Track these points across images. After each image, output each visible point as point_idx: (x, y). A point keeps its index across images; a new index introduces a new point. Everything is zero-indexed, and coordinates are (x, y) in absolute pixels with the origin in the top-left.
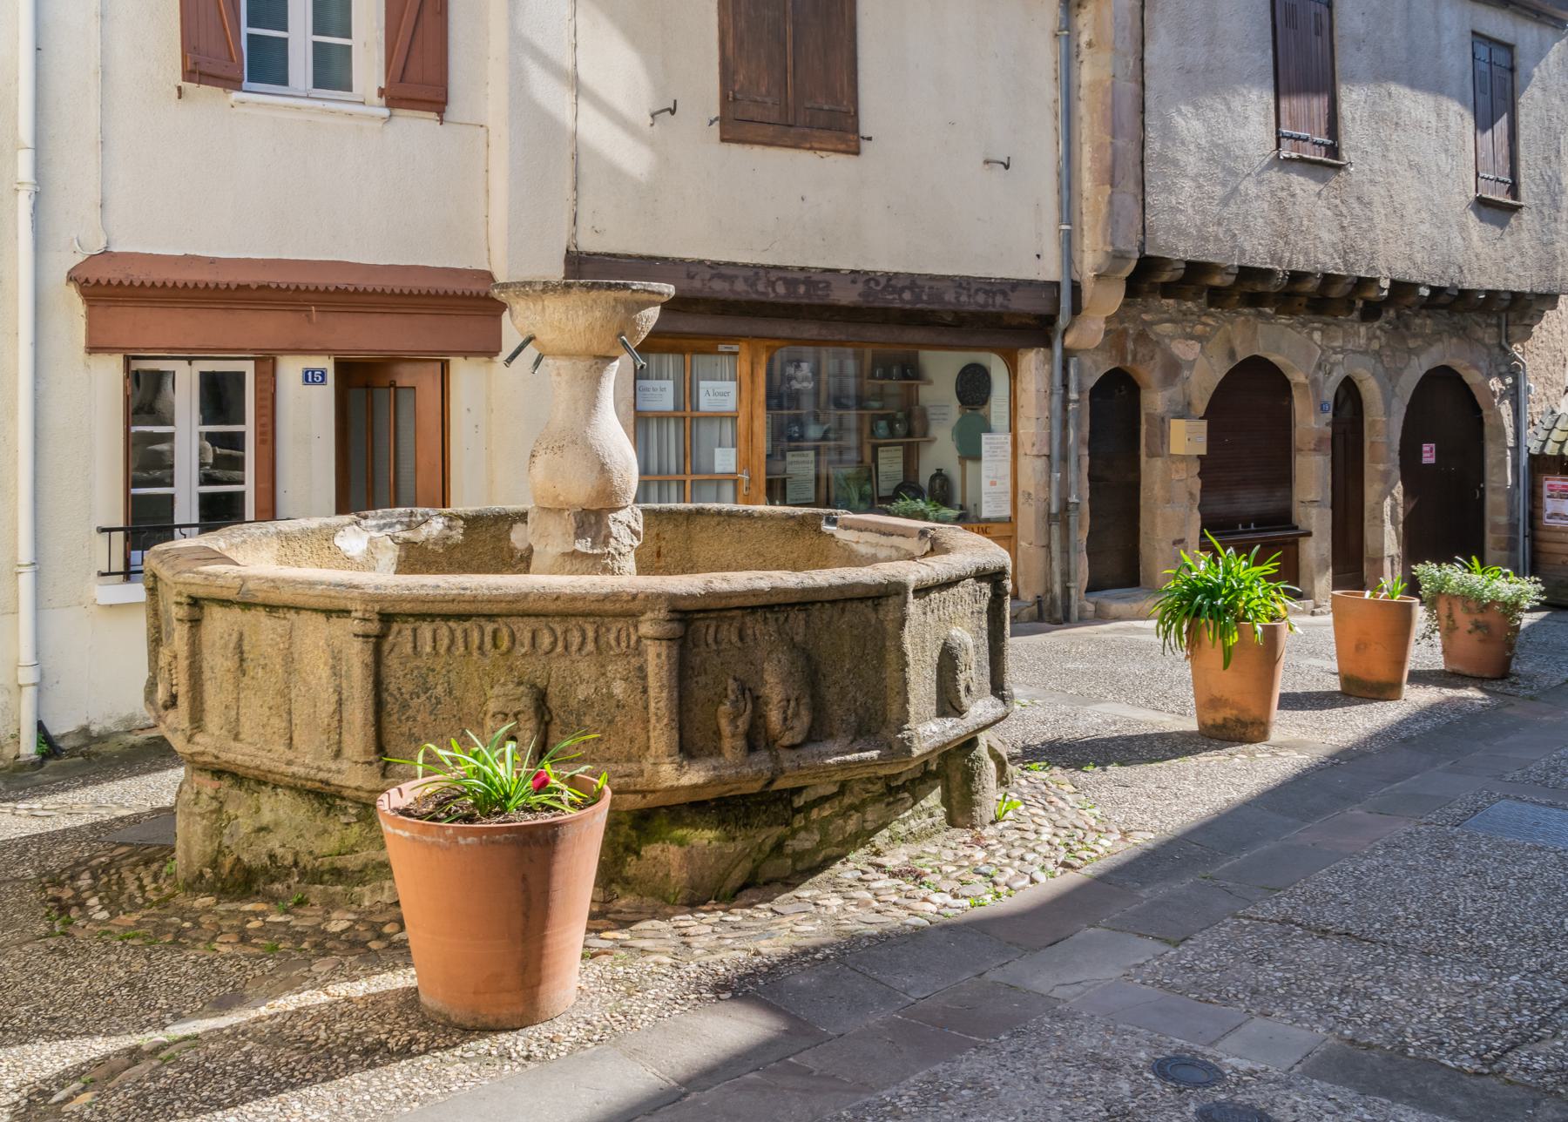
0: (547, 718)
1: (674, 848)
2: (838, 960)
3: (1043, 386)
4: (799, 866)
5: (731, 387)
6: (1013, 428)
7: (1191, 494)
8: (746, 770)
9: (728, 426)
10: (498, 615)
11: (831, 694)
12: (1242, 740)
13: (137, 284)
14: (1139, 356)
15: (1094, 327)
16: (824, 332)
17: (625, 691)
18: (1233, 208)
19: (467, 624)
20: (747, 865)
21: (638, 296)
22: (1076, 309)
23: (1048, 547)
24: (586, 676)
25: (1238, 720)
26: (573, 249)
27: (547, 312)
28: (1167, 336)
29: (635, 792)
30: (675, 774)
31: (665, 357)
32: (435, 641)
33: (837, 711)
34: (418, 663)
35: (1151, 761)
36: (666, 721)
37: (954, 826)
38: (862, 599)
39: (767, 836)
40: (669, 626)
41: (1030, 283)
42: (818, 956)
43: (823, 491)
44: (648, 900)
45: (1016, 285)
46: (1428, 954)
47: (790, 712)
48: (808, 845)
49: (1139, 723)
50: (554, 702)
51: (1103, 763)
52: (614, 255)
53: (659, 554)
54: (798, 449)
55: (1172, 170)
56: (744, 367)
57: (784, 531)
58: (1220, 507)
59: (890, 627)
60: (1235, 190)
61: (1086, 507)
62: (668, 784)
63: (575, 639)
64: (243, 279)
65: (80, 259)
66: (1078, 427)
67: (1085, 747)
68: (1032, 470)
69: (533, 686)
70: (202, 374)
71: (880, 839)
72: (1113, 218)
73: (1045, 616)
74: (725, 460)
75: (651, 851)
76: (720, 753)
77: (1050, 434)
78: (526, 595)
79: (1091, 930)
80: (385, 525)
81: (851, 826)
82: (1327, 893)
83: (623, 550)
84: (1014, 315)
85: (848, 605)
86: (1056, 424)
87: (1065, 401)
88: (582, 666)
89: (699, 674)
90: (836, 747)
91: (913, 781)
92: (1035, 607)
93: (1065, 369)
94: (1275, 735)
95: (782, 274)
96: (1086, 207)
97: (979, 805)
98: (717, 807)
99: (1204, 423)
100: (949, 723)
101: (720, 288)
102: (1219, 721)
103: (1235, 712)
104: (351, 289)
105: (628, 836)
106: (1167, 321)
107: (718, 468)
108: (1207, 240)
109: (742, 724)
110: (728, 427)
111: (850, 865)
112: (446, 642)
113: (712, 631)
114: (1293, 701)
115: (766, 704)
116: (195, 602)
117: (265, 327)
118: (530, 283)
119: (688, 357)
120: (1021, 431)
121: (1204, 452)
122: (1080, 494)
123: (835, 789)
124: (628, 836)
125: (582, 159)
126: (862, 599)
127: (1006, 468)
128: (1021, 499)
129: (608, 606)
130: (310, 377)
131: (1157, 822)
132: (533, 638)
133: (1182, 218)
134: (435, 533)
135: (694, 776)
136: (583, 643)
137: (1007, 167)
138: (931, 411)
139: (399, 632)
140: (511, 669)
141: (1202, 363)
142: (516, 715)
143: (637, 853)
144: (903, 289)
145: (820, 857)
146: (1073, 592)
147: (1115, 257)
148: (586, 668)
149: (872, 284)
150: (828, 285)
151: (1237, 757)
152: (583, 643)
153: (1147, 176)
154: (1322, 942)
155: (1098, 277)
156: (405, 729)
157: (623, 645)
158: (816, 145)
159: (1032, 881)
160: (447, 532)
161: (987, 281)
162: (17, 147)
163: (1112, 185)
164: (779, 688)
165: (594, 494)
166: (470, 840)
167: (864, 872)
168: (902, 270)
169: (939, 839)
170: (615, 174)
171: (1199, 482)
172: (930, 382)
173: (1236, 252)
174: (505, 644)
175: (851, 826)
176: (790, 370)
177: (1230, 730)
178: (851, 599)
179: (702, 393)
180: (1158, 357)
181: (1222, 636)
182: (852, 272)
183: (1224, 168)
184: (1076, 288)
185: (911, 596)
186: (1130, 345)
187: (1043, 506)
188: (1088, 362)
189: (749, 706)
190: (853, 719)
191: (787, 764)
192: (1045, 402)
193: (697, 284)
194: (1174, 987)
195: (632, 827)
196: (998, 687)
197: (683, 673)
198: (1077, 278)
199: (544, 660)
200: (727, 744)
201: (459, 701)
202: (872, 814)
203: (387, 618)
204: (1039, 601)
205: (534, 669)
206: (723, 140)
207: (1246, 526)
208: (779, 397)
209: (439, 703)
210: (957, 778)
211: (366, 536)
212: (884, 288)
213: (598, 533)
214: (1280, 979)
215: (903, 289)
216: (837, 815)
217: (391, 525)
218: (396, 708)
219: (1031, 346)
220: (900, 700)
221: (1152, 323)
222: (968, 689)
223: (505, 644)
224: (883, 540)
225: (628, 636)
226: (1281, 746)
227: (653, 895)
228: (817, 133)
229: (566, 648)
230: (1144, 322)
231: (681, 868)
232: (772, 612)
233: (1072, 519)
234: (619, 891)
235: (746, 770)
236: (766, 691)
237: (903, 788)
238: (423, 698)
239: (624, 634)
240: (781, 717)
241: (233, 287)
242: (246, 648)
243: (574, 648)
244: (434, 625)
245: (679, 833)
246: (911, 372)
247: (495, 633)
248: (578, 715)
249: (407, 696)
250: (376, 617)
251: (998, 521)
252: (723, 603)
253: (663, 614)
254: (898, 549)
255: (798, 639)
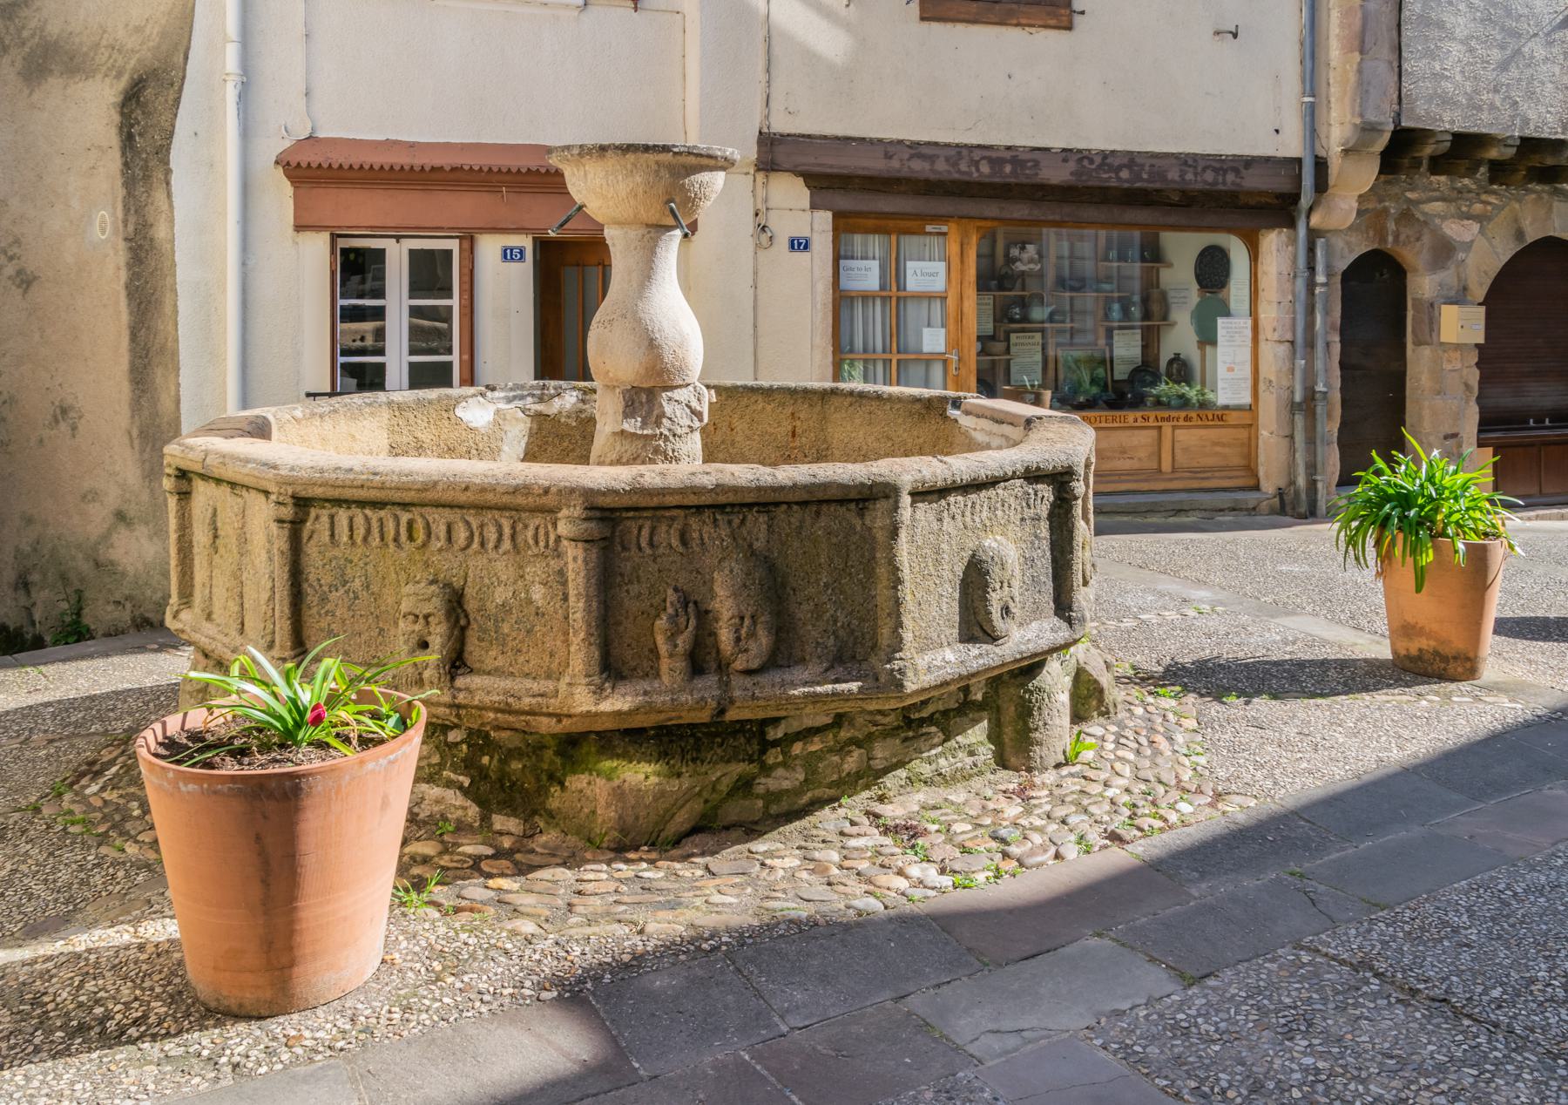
0: (463, 622)
1: (600, 782)
2: (726, 954)
3: (1286, 268)
4: (774, 809)
5: (941, 267)
6: (1254, 313)
7: (1467, 385)
8: (684, 697)
9: (937, 305)
10: (413, 505)
11: (803, 612)
12: (1443, 677)
13: (335, 166)
14: (1402, 237)
15: (1344, 206)
16: (1036, 212)
17: (544, 598)
18: (1514, 72)
19: (382, 513)
20: (697, 806)
21: (682, 159)
22: (1321, 185)
23: (1291, 437)
24: (504, 578)
25: (1436, 653)
26: (765, 130)
27: (590, 176)
28: (1439, 216)
29: (550, 715)
30: (591, 698)
31: (871, 237)
32: (351, 529)
33: (811, 632)
34: (336, 552)
35: (1313, 695)
36: (582, 635)
37: (1005, 767)
38: (842, 502)
39: (727, 773)
40: (585, 525)
41: (1268, 159)
42: (705, 946)
43: (1051, 373)
44: (572, 840)
45: (1250, 162)
46: (1556, 1057)
47: (743, 632)
48: (786, 785)
49: (1324, 642)
50: (471, 605)
51: (1247, 695)
52: (809, 136)
53: (794, 435)
54: (1023, 330)
55: (1436, 33)
56: (954, 248)
57: (911, 414)
58: (1505, 399)
59: (880, 536)
60: (1518, 52)
61: (1336, 396)
62: (584, 708)
63: (491, 535)
64: (457, 160)
65: (287, 144)
66: (1327, 312)
67: (1183, 682)
68: (1273, 356)
69: (448, 585)
70: (412, 252)
71: (891, 781)
72: (1363, 86)
73: (1288, 509)
74: (933, 340)
75: (577, 782)
76: (658, 675)
77: (1294, 319)
78: (436, 483)
79: (1094, 942)
80: (515, 398)
81: (852, 762)
82: (1446, 924)
83: (679, 431)
84: (1250, 193)
85: (824, 508)
86: (1300, 309)
87: (1311, 285)
88: (500, 565)
89: (631, 582)
90: (806, 676)
91: (945, 713)
92: (1277, 500)
93: (1311, 250)
94: (1490, 670)
95: (987, 153)
96: (1333, 77)
97: (1040, 744)
98: (657, 736)
99: (1483, 309)
100: (975, 650)
101: (919, 167)
102: (1414, 652)
103: (1432, 643)
104: (543, 171)
105: (552, 762)
106: (1437, 200)
107: (926, 349)
108: (1480, 109)
109: (683, 642)
110: (937, 306)
111: (841, 812)
112: (392, 533)
113: (645, 532)
114: (1513, 628)
115: (717, 620)
116: (183, 475)
117: (463, 206)
118: (568, 148)
119: (894, 238)
120: (1262, 316)
121: (1482, 341)
122: (1330, 382)
123: (828, 720)
124: (552, 762)
125: (773, 43)
126: (842, 502)
127: (1246, 354)
128: (1262, 387)
129: (520, 500)
130: (508, 254)
131: (1269, 784)
132: (449, 531)
133: (1449, 86)
134: (568, 406)
135: (619, 702)
136: (500, 540)
137: (1235, 36)
138: (1171, 294)
139: (317, 518)
140: (427, 565)
141: (1481, 243)
142: (426, 617)
143: (561, 784)
144: (1120, 168)
145: (805, 799)
146: (1320, 485)
147: (1363, 129)
148: (503, 568)
149: (1086, 162)
150: (1036, 164)
151: (1426, 699)
152: (500, 540)
153: (1404, 40)
154: (1399, 1010)
155: (1346, 152)
156: (323, 624)
157: (542, 544)
158: (1023, 21)
159: (1057, 856)
160: (581, 405)
161: (1217, 158)
162: (226, 40)
163: (1361, 52)
164: (729, 603)
165: (642, 371)
166: (191, 787)
167: (853, 823)
168: (1118, 148)
169: (977, 783)
170: (811, 58)
171: (1477, 372)
172: (1170, 265)
173: (1518, 121)
174: (420, 536)
175: (852, 762)
176: (1015, 252)
177: (1427, 665)
178: (828, 502)
179: (909, 273)
180: (1426, 239)
181: (1414, 552)
182: (1064, 150)
183: (1503, 29)
184: (1321, 165)
185: (906, 500)
186: (1391, 226)
187: (1286, 394)
188: (1339, 243)
189: (693, 622)
190: (831, 641)
191: (737, 693)
192: (1288, 286)
193: (895, 164)
194: (1144, 1060)
195: (557, 753)
196: (1063, 606)
197: (607, 582)
198: (1322, 153)
199: (461, 557)
200: (665, 664)
201: (377, 597)
202: (882, 752)
203: (302, 503)
204: (1281, 493)
205: (449, 565)
206: (923, 19)
207: (1539, 420)
208: (995, 278)
209: (356, 598)
210: (1010, 711)
211: (492, 408)
212: (1100, 167)
213: (650, 412)
214: (1306, 1070)
215: (1120, 168)
216: (830, 750)
217: (522, 398)
218: (316, 600)
219: (1272, 227)
220: (891, 623)
221: (1418, 202)
222: (1006, 611)
223: (420, 536)
224: (995, 428)
225: (547, 534)
226: (1492, 688)
227: (577, 833)
228: (1023, 8)
229: (482, 544)
230: (1410, 201)
231: (608, 805)
232: (723, 513)
233: (1319, 410)
234: (542, 824)
235: (684, 697)
236: (715, 605)
237: (930, 720)
238: (342, 591)
239: (542, 531)
240: (732, 636)
241: (427, 169)
242: (219, 525)
243: (491, 545)
244: (350, 513)
245: (607, 764)
246: (1153, 255)
247: (410, 524)
248: (496, 621)
249: (326, 589)
250: (289, 501)
251: (1239, 408)
252: (655, 502)
253: (578, 512)
254: (1007, 438)
255: (757, 545)
